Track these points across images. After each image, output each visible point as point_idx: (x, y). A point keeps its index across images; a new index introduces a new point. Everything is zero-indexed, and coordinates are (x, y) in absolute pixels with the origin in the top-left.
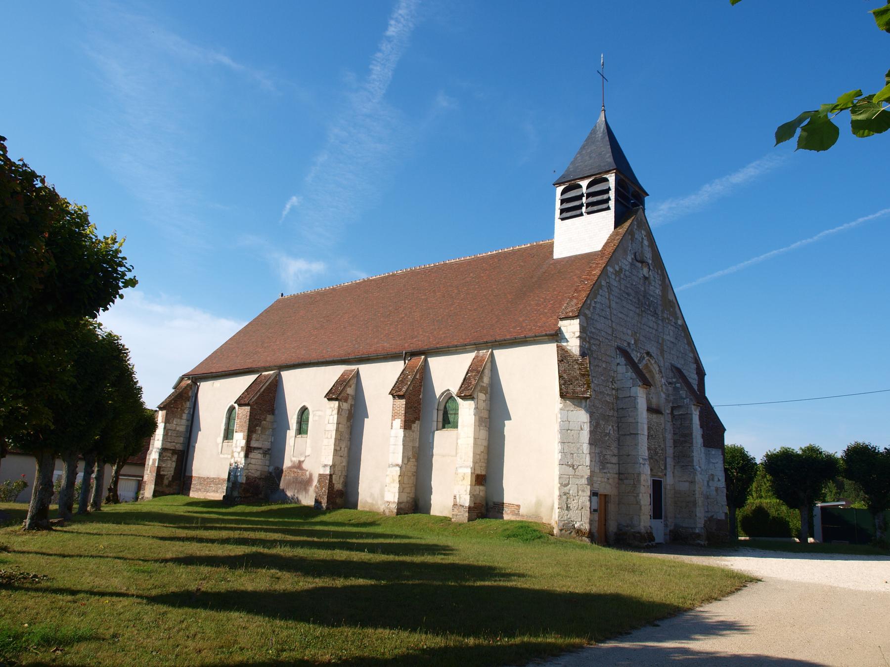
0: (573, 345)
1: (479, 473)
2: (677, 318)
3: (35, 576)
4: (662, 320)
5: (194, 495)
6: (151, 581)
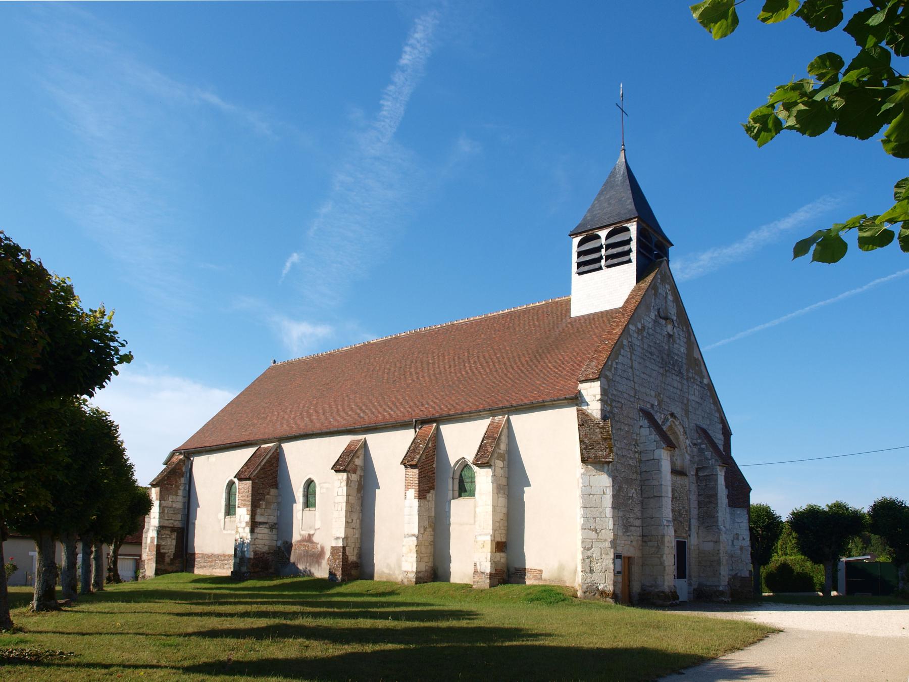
0: (594, 408)
1: (499, 540)
2: (702, 377)
3: (62, 653)
4: (687, 380)
5: (199, 571)
6: (181, 653)
